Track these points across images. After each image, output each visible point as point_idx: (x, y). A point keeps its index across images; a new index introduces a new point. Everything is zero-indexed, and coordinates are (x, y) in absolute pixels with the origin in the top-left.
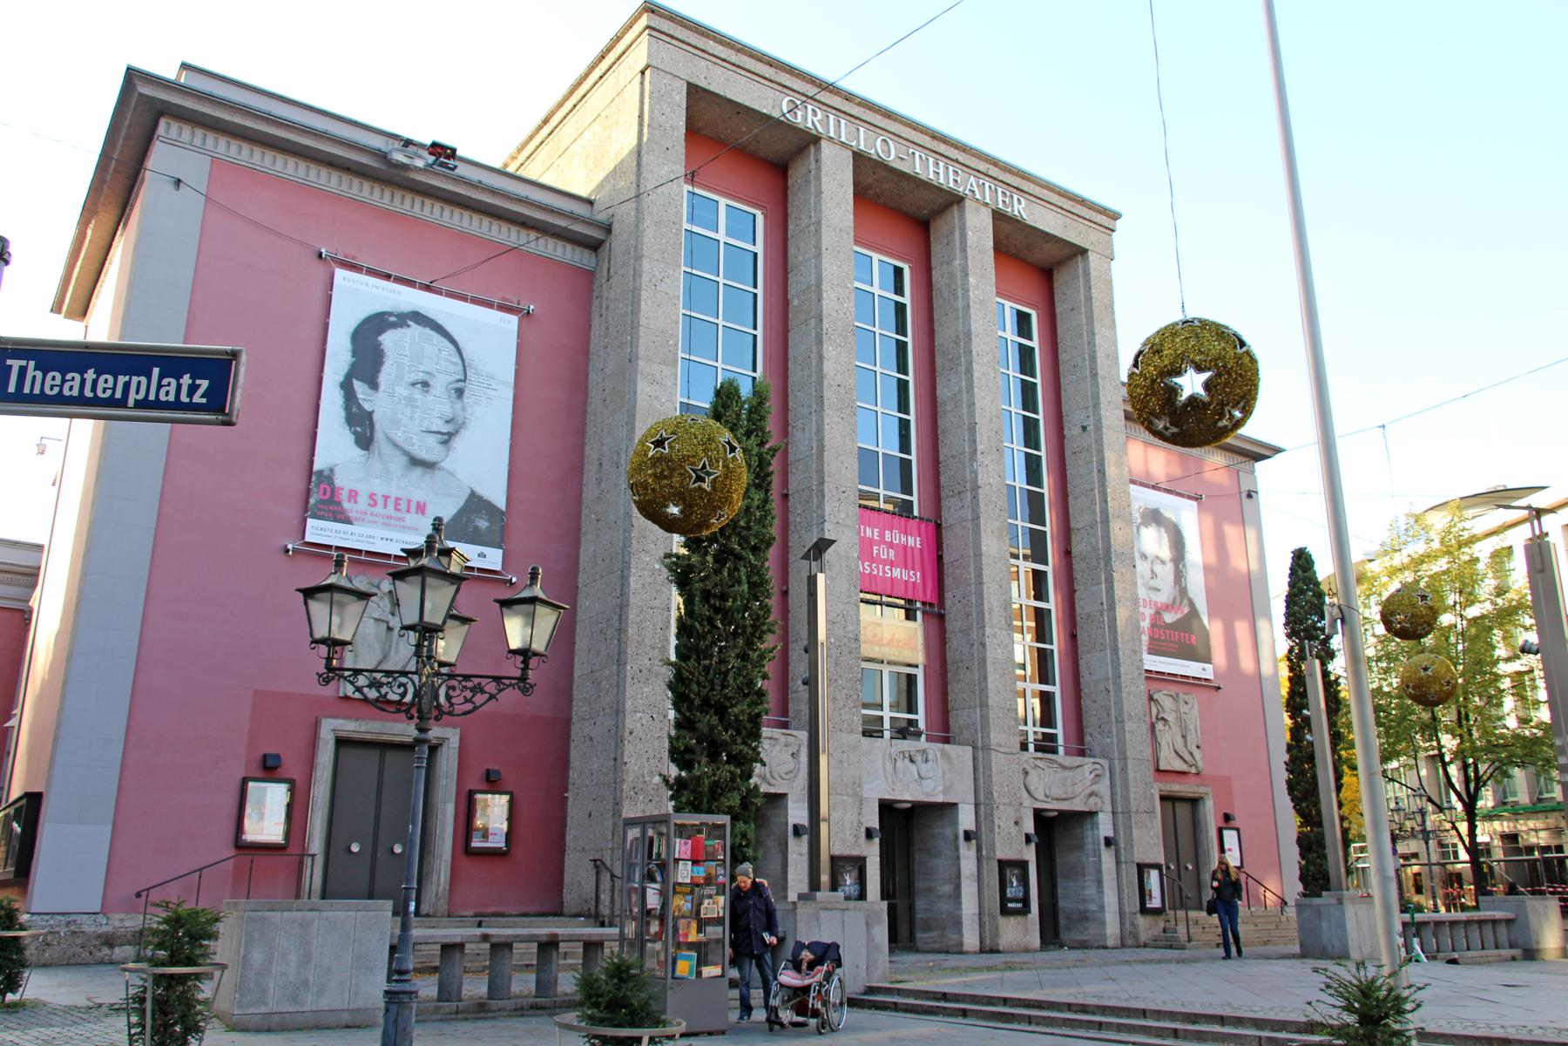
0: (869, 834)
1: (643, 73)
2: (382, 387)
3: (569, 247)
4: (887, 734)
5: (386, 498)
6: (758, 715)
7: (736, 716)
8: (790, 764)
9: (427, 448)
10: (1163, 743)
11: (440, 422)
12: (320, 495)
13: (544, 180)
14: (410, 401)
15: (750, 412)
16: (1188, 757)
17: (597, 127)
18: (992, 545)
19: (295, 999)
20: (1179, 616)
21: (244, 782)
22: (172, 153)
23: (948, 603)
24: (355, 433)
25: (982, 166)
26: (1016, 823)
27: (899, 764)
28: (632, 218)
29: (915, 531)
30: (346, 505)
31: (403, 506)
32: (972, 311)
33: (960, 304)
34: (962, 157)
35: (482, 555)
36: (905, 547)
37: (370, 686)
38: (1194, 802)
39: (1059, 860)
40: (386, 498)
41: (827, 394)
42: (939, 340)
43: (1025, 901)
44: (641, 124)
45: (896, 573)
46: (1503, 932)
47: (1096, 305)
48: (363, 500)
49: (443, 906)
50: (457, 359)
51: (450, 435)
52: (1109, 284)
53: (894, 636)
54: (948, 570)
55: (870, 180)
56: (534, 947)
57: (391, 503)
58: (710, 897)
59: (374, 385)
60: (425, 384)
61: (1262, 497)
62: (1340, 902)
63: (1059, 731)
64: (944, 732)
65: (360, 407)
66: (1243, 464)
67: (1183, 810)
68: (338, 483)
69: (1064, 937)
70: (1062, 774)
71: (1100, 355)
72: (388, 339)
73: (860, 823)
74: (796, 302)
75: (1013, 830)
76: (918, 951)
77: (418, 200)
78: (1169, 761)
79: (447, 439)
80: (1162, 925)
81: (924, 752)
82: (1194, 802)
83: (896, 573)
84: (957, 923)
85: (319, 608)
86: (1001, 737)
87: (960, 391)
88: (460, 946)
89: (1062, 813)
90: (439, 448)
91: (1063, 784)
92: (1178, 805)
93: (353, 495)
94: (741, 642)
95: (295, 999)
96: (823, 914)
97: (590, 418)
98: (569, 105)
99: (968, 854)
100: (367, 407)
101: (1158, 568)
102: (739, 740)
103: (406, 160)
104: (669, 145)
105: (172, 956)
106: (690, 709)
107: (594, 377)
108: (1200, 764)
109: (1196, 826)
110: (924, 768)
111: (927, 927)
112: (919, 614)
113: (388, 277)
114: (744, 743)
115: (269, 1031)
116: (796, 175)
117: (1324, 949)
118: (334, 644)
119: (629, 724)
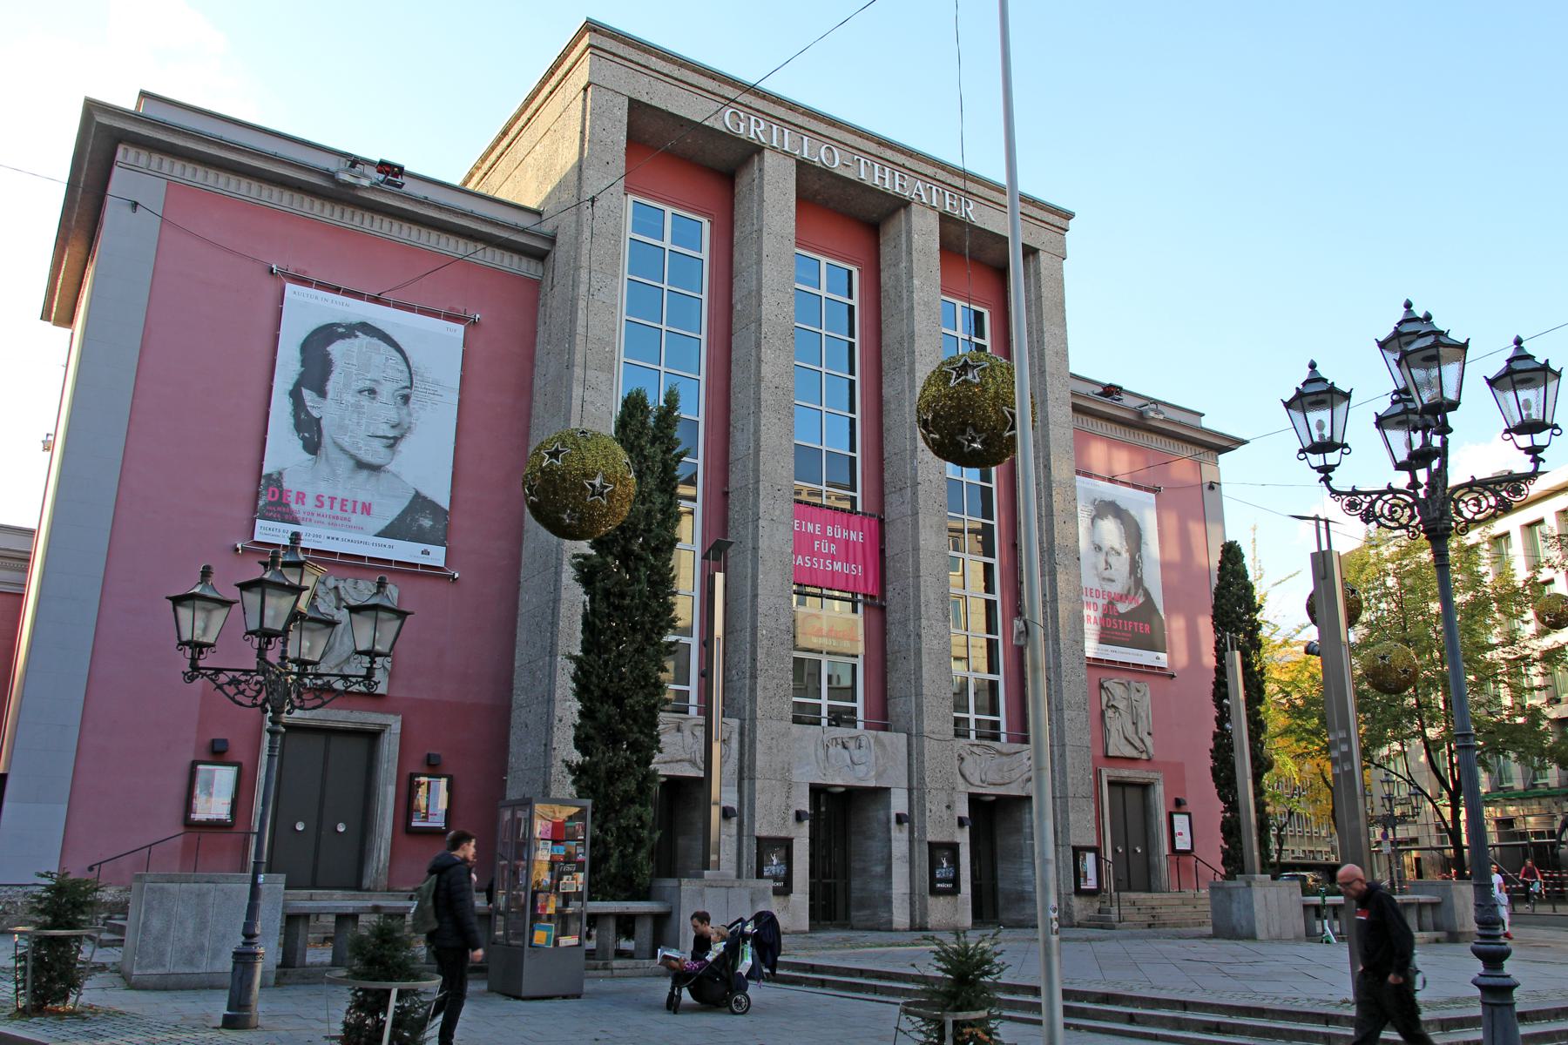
0: (799, 816)
1: (585, 89)
2: (330, 395)
3: (516, 258)
4: (824, 722)
5: (333, 499)
6: (655, 706)
7: (632, 707)
9: (373, 452)
10: (1113, 730)
11: (385, 427)
12: (271, 498)
13: (500, 195)
14: (358, 408)
15: (658, 419)
16: (1138, 743)
17: (546, 141)
18: (931, 540)
19: (190, 962)
20: (1133, 605)
21: (194, 765)
22: (133, 179)
23: (889, 595)
24: (303, 438)
25: (930, 171)
26: (948, 807)
27: (832, 750)
28: (573, 231)
29: (858, 526)
30: (293, 506)
31: (349, 507)
32: (916, 312)
33: (905, 306)
34: (909, 162)
35: (425, 552)
36: (847, 541)
37: (229, 684)
38: (1145, 787)
39: (1000, 842)
40: (333, 499)
41: (764, 395)
42: (886, 339)
43: (956, 881)
44: (582, 140)
45: (838, 566)
46: (1428, 915)
47: (1046, 304)
48: (310, 502)
49: (383, 880)
50: (404, 368)
52: (1060, 283)
53: (833, 625)
54: (889, 563)
55: (817, 187)
56: (332, 919)
57: (337, 505)
58: (570, 873)
59: (322, 394)
60: (372, 392)
61: (1225, 489)
62: (1249, 885)
63: (1002, 719)
64: (882, 719)
65: (308, 414)
66: (1206, 456)
67: (1133, 796)
68: (286, 485)
69: (1003, 916)
70: (998, 759)
71: (1049, 352)
72: (337, 349)
73: (788, 807)
74: (739, 307)
75: (945, 814)
76: (852, 929)
77: (367, 216)
78: (1118, 747)
79: (393, 443)
80: (1097, 905)
81: (857, 738)
82: (1145, 787)
83: (838, 566)
84: (888, 902)
85: (185, 613)
86: (937, 720)
87: (903, 391)
88: (354, 917)
89: (1000, 798)
90: (383, 451)
91: (993, 771)
92: (1128, 791)
93: (301, 497)
94: (639, 637)
95: (190, 962)
96: (708, 891)
97: (534, 421)
98: (524, 118)
99: (899, 840)
100: (315, 414)
101: (1113, 560)
102: (635, 729)
103: (352, 180)
104: (609, 159)
105: (54, 921)
106: (590, 700)
107: (538, 382)
108: (1151, 751)
109: (1147, 811)
110: (856, 754)
111: (862, 905)
112: (860, 607)
113: (337, 290)
114: (641, 732)
115: (166, 989)
116: (742, 183)
117: (1234, 929)
118: (198, 647)
119: (558, 712)
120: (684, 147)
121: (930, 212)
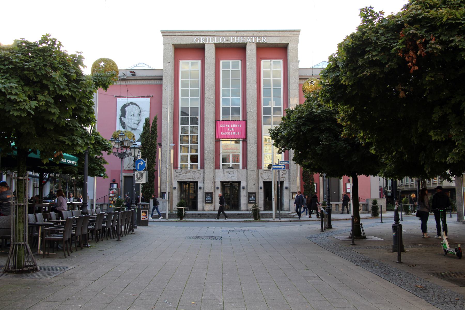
0: (261, 188)
8: (199, 176)
14: (131, 118)
25: (252, 33)
45: (234, 133)
51: (138, 123)
59: (125, 117)
60: (133, 115)
83: (234, 133)
120: (186, 49)
121: (253, 44)
